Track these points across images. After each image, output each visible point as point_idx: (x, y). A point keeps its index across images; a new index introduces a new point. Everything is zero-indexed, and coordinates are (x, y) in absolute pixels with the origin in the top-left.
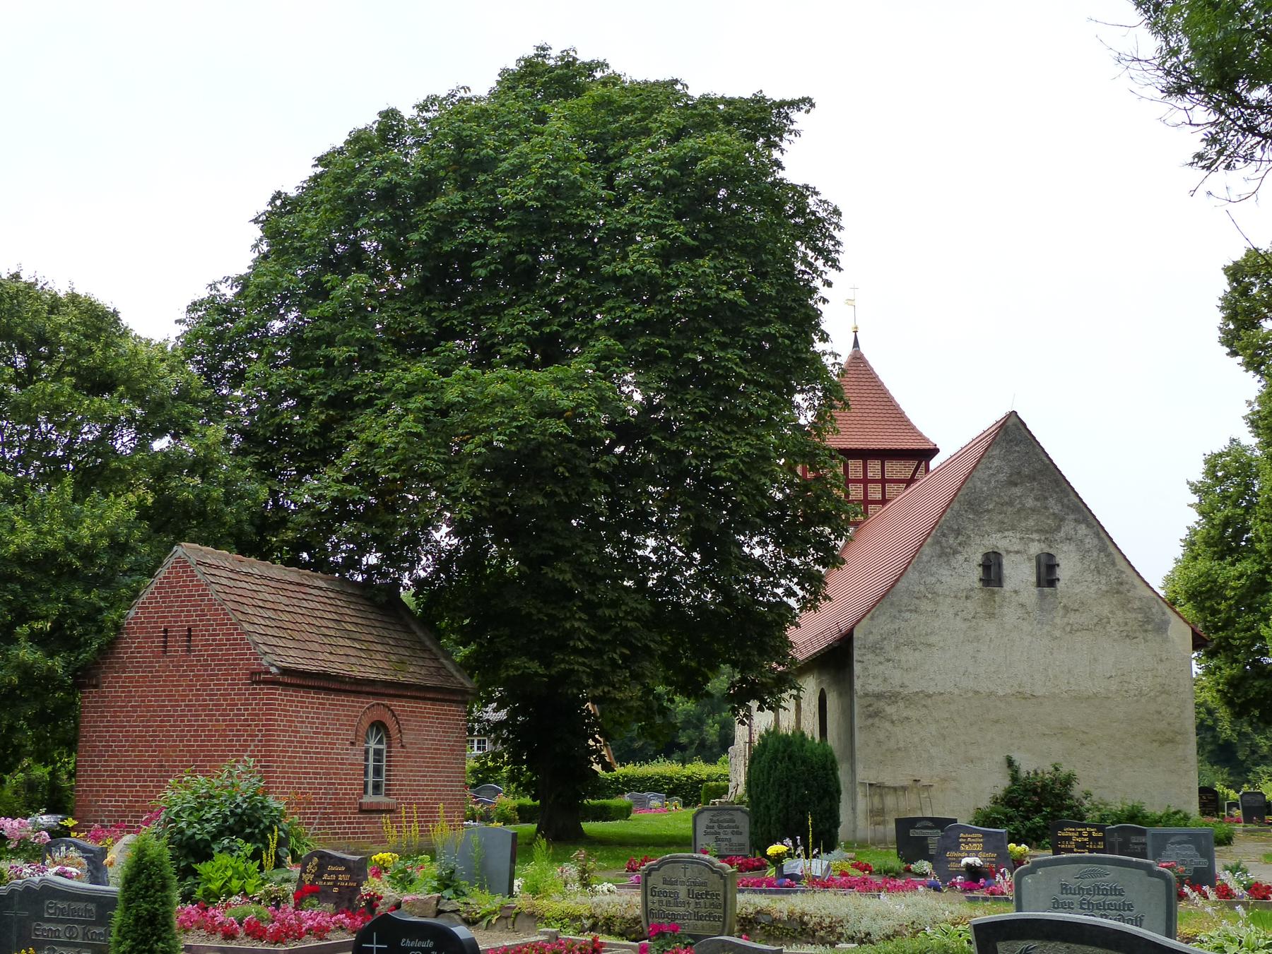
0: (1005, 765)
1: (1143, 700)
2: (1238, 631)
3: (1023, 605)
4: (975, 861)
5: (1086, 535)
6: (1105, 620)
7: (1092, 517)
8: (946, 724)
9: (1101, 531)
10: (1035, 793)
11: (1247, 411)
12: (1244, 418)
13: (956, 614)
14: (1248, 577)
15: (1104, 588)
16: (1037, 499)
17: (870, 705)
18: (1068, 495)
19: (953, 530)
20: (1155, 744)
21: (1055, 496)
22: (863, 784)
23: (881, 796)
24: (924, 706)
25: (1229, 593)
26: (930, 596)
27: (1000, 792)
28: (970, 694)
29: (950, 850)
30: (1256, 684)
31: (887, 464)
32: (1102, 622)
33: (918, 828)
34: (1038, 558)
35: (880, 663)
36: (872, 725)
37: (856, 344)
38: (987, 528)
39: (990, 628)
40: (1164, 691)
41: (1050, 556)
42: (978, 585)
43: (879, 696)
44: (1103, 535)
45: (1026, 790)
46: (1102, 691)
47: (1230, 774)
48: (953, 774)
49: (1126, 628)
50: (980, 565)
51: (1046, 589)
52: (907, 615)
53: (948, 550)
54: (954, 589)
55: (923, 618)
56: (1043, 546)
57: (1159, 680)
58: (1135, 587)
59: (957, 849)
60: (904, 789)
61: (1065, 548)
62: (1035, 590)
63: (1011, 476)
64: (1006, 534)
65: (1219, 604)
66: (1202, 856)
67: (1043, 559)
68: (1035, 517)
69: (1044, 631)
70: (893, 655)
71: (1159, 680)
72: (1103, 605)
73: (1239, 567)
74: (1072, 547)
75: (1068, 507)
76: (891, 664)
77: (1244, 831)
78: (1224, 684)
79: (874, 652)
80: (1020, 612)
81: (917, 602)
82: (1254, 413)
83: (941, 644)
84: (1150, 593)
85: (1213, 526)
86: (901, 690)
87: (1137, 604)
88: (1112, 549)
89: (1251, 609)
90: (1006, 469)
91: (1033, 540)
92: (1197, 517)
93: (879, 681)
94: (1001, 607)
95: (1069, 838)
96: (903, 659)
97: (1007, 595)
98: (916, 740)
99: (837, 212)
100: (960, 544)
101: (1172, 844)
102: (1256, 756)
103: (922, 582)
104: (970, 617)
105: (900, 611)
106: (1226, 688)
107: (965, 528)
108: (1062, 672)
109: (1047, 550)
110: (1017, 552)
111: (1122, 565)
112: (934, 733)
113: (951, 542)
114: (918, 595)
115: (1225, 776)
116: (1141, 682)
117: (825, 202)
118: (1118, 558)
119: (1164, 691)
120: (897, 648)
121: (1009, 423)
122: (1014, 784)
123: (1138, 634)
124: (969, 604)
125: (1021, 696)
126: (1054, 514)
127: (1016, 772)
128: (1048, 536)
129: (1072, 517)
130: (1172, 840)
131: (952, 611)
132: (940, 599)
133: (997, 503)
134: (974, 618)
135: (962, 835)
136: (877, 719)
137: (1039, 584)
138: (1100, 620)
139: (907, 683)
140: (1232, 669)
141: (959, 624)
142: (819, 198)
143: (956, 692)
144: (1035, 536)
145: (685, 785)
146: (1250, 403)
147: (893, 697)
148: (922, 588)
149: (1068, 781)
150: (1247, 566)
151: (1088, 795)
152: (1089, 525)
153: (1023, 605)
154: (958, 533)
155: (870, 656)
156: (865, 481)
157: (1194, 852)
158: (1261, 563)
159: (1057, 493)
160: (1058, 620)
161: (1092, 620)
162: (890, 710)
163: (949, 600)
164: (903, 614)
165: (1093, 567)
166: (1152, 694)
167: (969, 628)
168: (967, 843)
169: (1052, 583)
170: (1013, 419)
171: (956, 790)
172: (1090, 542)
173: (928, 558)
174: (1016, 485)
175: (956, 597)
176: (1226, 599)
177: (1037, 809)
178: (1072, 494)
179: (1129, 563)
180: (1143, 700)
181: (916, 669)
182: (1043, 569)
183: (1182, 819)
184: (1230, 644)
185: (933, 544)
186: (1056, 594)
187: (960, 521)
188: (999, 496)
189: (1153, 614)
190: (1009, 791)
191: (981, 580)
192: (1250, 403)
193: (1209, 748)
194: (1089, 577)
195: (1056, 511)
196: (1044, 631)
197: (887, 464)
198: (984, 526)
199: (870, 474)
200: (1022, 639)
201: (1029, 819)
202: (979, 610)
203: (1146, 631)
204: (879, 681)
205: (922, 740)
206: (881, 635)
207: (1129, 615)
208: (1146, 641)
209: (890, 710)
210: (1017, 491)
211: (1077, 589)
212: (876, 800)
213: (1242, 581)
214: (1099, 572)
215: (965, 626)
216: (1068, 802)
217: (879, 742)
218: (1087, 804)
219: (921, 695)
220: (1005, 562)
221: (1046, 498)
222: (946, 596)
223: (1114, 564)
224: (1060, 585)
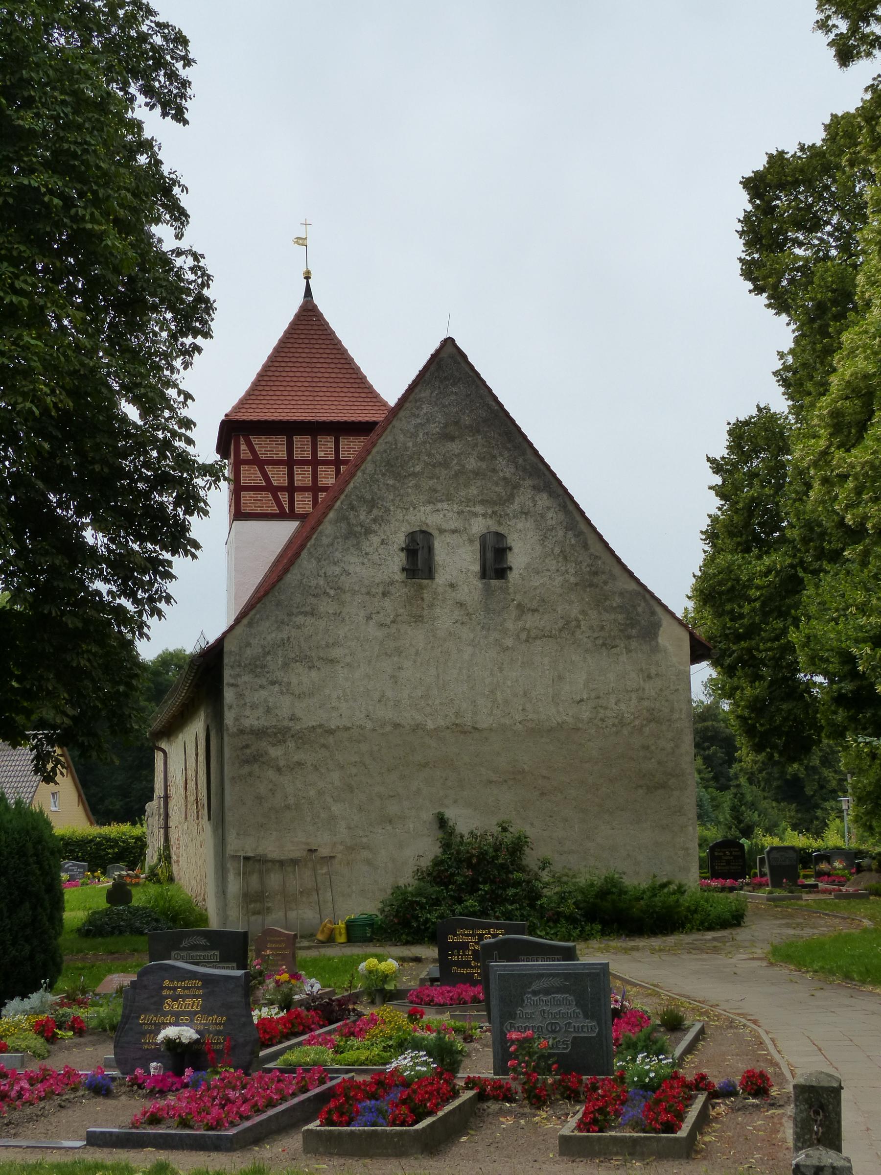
0: (436, 826)
1: (625, 732)
2: (765, 641)
3: (461, 605)
4: (186, 1033)
5: (549, 508)
6: (574, 623)
7: (555, 484)
8: (354, 770)
9: (569, 503)
10: (470, 866)
11: (778, 365)
12: (775, 374)
13: (369, 618)
14: (778, 573)
15: (572, 580)
16: (482, 459)
17: (247, 746)
18: (524, 453)
19: (365, 501)
20: (641, 791)
21: (506, 454)
22: (235, 858)
23: (261, 872)
24: (324, 746)
25: (754, 593)
26: (332, 592)
27: (426, 863)
28: (388, 729)
29: (146, 1010)
30: (784, 706)
31: (343, 442)
32: (569, 626)
33: (185, 949)
34: (483, 538)
35: (262, 687)
36: (250, 774)
37: (308, 292)
38: (413, 497)
39: (416, 636)
40: (653, 718)
41: (500, 536)
42: (399, 577)
43: (260, 733)
44: (571, 507)
45: (460, 861)
46: (569, 720)
47: (797, 811)
48: (365, 840)
49: (602, 634)
50: (402, 550)
51: (494, 582)
52: (300, 619)
53: (358, 529)
54: (366, 582)
55: (322, 624)
56: (490, 522)
57: (646, 703)
58: (613, 577)
59: (158, 1008)
60: (294, 862)
61: (520, 526)
62: (479, 584)
63: (446, 426)
64: (439, 506)
65: (741, 607)
66: (586, 1016)
67: (490, 542)
68: (479, 483)
69: (491, 639)
70: (279, 675)
71: (646, 703)
72: (571, 603)
73: (767, 560)
74: (530, 524)
75: (524, 470)
76: (276, 688)
77: (769, 900)
78: (746, 707)
79: (252, 671)
80: (457, 614)
81: (314, 601)
82: (786, 368)
83: (348, 659)
84: (633, 586)
85: (736, 511)
86: (291, 724)
87: (617, 601)
88: (583, 526)
89: (783, 614)
90: (439, 417)
91: (475, 515)
92: (719, 502)
93: (260, 711)
94: (431, 606)
95: (464, 946)
96: (294, 681)
97: (440, 590)
98: (312, 793)
99: (181, 40)
100: (375, 520)
101: (535, 993)
102: (824, 791)
103: (322, 573)
104: (388, 621)
105: (290, 614)
106: (746, 713)
107: (382, 499)
108: (516, 695)
109: (495, 528)
110: (454, 531)
111: (596, 549)
112: (337, 783)
113: (362, 517)
114: (316, 592)
115: (792, 814)
116: (623, 706)
117: (166, 26)
118: (591, 539)
119: (653, 718)
120: (285, 665)
121: (443, 355)
122: (444, 852)
123: (618, 641)
124: (387, 603)
125: (460, 729)
126: (505, 479)
127: (451, 834)
128: (496, 508)
129: (528, 482)
130: (534, 987)
131: (362, 613)
132: (347, 597)
133: (427, 464)
134: (393, 622)
135: (167, 983)
136: (256, 766)
137: (484, 574)
138: (568, 623)
139: (299, 713)
140: (755, 688)
141: (372, 631)
142: (157, 19)
143: (369, 725)
144: (479, 509)
145: (133, 848)
146: (781, 355)
147: (280, 735)
148: (321, 582)
149: (518, 847)
150: (776, 559)
151: (545, 864)
152: (552, 494)
153: (461, 605)
154: (372, 504)
155: (246, 678)
156: (315, 463)
157: (573, 1009)
158: (794, 556)
159: (509, 450)
160: (510, 625)
161: (556, 623)
162: (275, 752)
163: (359, 599)
164: (294, 619)
165: (557, 550)
166: (637, 722)
167: (388, 636)
168: (175, 999)
169: (501, 572)
170: (449, 349)
171: (369, 862)
172: (553, 517)
173: (329, 540)
174: (452, 439)
175: (368, 593)
176: (750, 601)
177: (472, 887)
178: (529, 451)
179: (606, 544)
180: (625, 732)
181: (311, 695)
182: (490, 555)
183: (674, 893)
184: (753, 657)
185: (337, 521)
186: (507, 588)
187: (375, 488)
188: (429, 455)
189: (638, 615)
190: (437, 863)
191: (404, 569)
192: (781, 355)
193: (775, 784)
194: (552, 564)
195: (508, 475)
196: (491, 639)
197: (343, 442)
198: (408, 495)
199: (321, 454)
200: (459, 651)
201: (460, 901)
202: (401, 611)
203: (629, 637)
204: (260, 711)
205: (321, 793)
206: (263, 647)
207: (606, 616)
208: (629, 651)
209: (275, 752)
210: (454, 447)
211: (536, 581)
212: (254, 879)
213: (770, 578)
214: (565, 558)
215: (380, 634)
216: (516, 875)
217: (259, 798)
218: (545, 876)
219: (319, 730)
220: (437, 545)
221: (494, 457)
222: (354, 593)
223: (586, 547)
224: (513, 576)
